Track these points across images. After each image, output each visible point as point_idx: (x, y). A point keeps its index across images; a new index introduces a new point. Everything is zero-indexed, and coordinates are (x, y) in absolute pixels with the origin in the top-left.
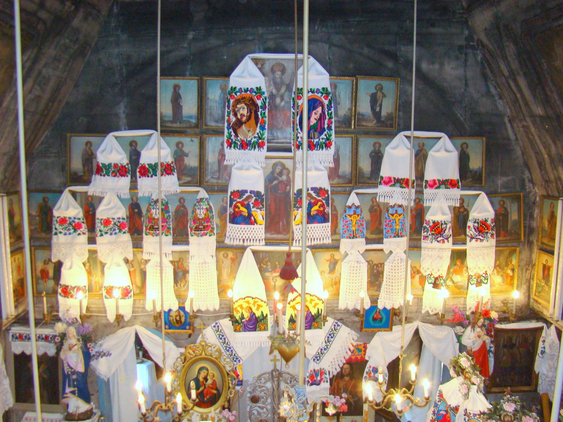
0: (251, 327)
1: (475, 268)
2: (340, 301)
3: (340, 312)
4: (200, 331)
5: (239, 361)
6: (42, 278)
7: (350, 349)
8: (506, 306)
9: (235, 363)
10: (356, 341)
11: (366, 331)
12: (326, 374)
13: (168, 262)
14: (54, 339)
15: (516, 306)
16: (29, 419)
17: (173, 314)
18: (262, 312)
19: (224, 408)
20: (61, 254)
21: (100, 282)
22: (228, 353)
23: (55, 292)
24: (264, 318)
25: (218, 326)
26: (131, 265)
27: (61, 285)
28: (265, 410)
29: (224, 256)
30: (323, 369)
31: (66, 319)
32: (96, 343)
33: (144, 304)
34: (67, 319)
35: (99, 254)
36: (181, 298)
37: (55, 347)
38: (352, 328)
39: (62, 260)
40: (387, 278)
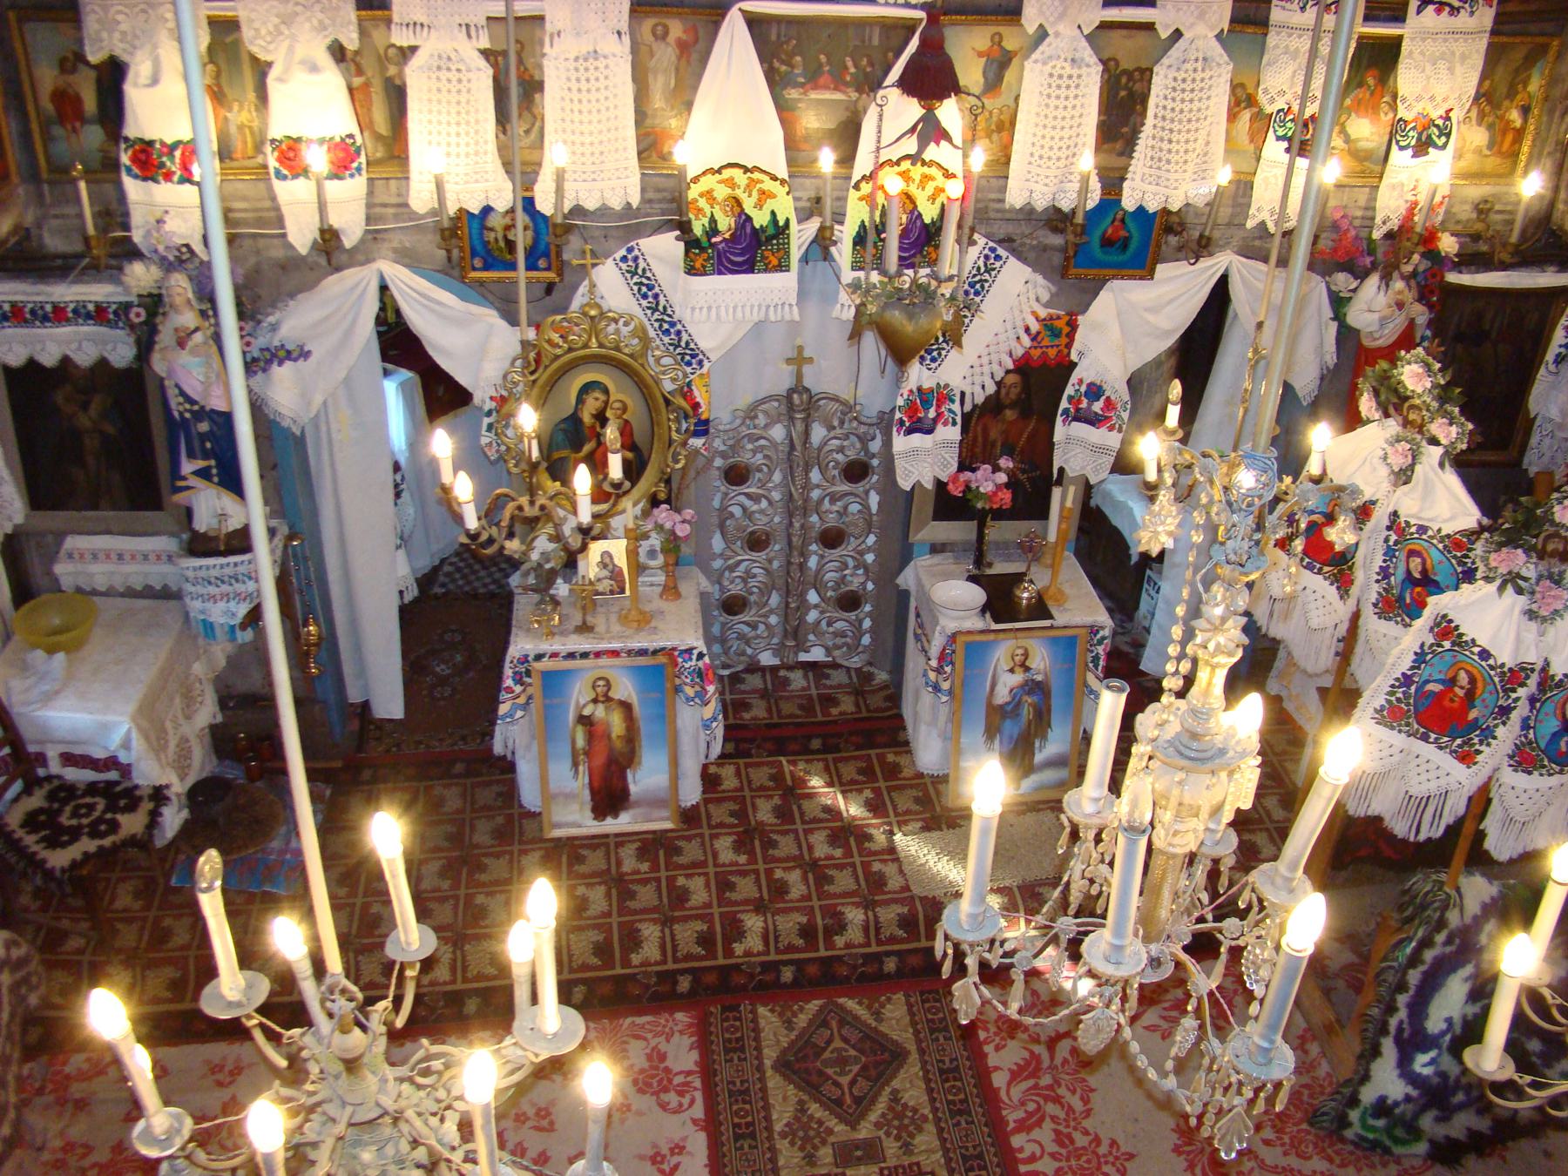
0: (740, 259)
1: (1419, 99)
2: (1010, 181)
3: (1008, 216)
4: (583, 271)
5: (700, 363)
6: (62, 119)
7: (1027, 330)
8: (1483, 221)
9: (689, 370)
10: (1046, 306)
11: (1078, 277)
12: (953, 401)
13: (477, 54)
14: (127, 315)
15: (1527, 211)
16: (76, 556)
17: (495, 221)
18: (773, 213)
19: (654, 502)
20: (117, 35)
21: (256, 124)
22: (666, 340)
23: (113, 166)
24: (780, 231)
25: (636, 259)
26: (353, 68)
27: (127, 139)
28: (764, 504)
29: (654, 34)
30: (947, 386)
31: (156, 251)
32: (259, 322)
33: (404, 192)
34: (161, 248)
35: (247, 33)
36: (522, 170)
37: (132, 340)
38: (1035, 266)
39: (125, 58)
40: (1156, 116)
